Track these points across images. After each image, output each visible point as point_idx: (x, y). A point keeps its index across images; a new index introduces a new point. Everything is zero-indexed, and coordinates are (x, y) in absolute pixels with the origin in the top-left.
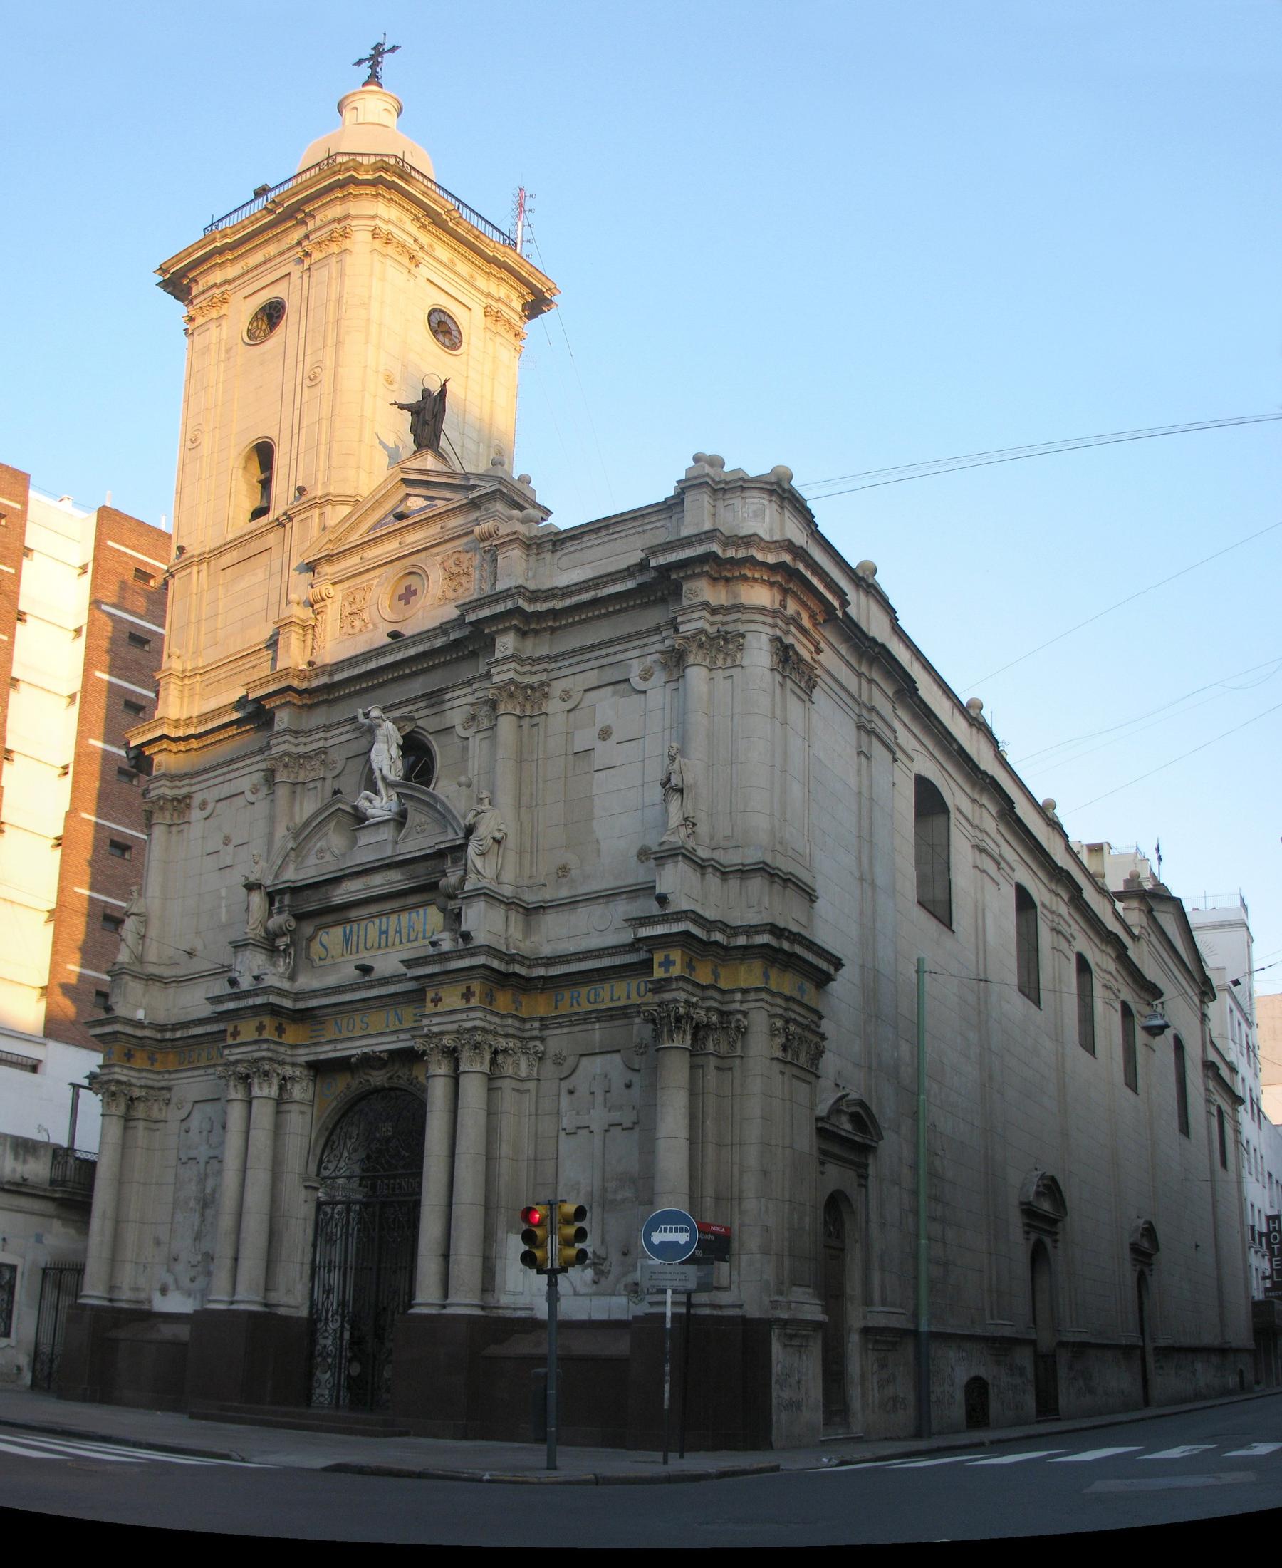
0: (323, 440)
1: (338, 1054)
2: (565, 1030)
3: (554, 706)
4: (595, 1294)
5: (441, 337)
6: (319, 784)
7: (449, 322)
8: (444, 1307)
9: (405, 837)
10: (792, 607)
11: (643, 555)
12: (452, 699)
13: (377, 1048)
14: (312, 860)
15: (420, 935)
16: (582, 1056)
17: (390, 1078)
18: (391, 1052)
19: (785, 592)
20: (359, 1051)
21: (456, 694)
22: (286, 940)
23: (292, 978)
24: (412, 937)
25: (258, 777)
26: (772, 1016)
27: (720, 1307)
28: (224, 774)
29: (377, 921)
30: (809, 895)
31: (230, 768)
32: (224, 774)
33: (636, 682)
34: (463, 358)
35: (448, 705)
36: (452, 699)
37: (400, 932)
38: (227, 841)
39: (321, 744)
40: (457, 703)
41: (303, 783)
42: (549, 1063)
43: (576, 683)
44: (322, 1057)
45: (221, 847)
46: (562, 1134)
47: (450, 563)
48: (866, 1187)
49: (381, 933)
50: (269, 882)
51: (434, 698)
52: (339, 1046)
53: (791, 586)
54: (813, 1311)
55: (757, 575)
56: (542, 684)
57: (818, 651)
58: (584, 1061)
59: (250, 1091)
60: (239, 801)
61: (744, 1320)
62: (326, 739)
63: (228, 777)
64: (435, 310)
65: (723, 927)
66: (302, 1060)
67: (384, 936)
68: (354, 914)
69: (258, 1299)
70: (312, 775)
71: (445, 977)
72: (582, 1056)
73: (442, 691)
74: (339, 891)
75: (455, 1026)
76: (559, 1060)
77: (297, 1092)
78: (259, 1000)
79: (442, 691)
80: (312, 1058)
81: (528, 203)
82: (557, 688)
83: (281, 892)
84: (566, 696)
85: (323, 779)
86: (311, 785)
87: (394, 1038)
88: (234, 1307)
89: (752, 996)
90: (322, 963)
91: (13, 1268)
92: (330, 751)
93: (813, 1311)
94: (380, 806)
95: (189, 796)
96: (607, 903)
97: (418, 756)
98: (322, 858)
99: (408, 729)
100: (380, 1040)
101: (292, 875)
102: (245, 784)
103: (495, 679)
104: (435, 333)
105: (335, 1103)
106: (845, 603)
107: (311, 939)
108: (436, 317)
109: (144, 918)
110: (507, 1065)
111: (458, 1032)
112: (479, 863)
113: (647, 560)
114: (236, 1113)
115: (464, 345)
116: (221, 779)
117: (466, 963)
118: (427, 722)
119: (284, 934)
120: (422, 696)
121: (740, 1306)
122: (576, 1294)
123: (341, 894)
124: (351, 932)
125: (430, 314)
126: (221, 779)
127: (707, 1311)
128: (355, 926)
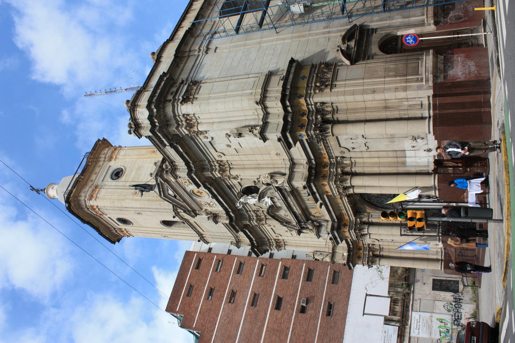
0: (162, 193)
2: (332, 151)
4: (427, 139)
5: (120, 175)
7: (115, 173)
8: (435, 188)
10: (170, 97)
13: (347, 201)
16: (340, 146)
19: (166, 101)
20: (349, 206)
23: (327, 221)
26: (315, 93)
27: (429, 104)
30: (270, 75)
33: (210, 139)
34: (126, 166)
42: (344, 155)
43: (215, 154)
46: (368, 150)
47: (186, 184)
48: (376, 29)
53: (162, 100)
54: (428, 61)
55: (162, 113)
57: (183, 81)
58: (342, 145)
59: (366, 234)
60: (274, 228)
61: (434, 96)
64: (112, 178)
65: (285, 119)
66: (354, 218)
68: (304, 207)
70: (262, 214)
72: (340, 146)
74: (297, 212)
75: (336, 189)
76: (342, 152)
77: (365, 219)
81: (89, 93)
89: (309, 102)
91: (434, 280)
93: (428, 61)
94: (267, 201)
95: (275, 240)
97: (249, 191)
99: (242, 194)
101: (294, 222)
102: (269, 228)
104: (119, 177)
106: (164, 74)
107: (314, 216)
108: (114, 177)
109: (315, 253)
110: (348, 169)
112: (280, 183)
115: (122, 167)
121: (429, 97)
122: (427, 144)
125: (113, 179)
127: (431, 111)
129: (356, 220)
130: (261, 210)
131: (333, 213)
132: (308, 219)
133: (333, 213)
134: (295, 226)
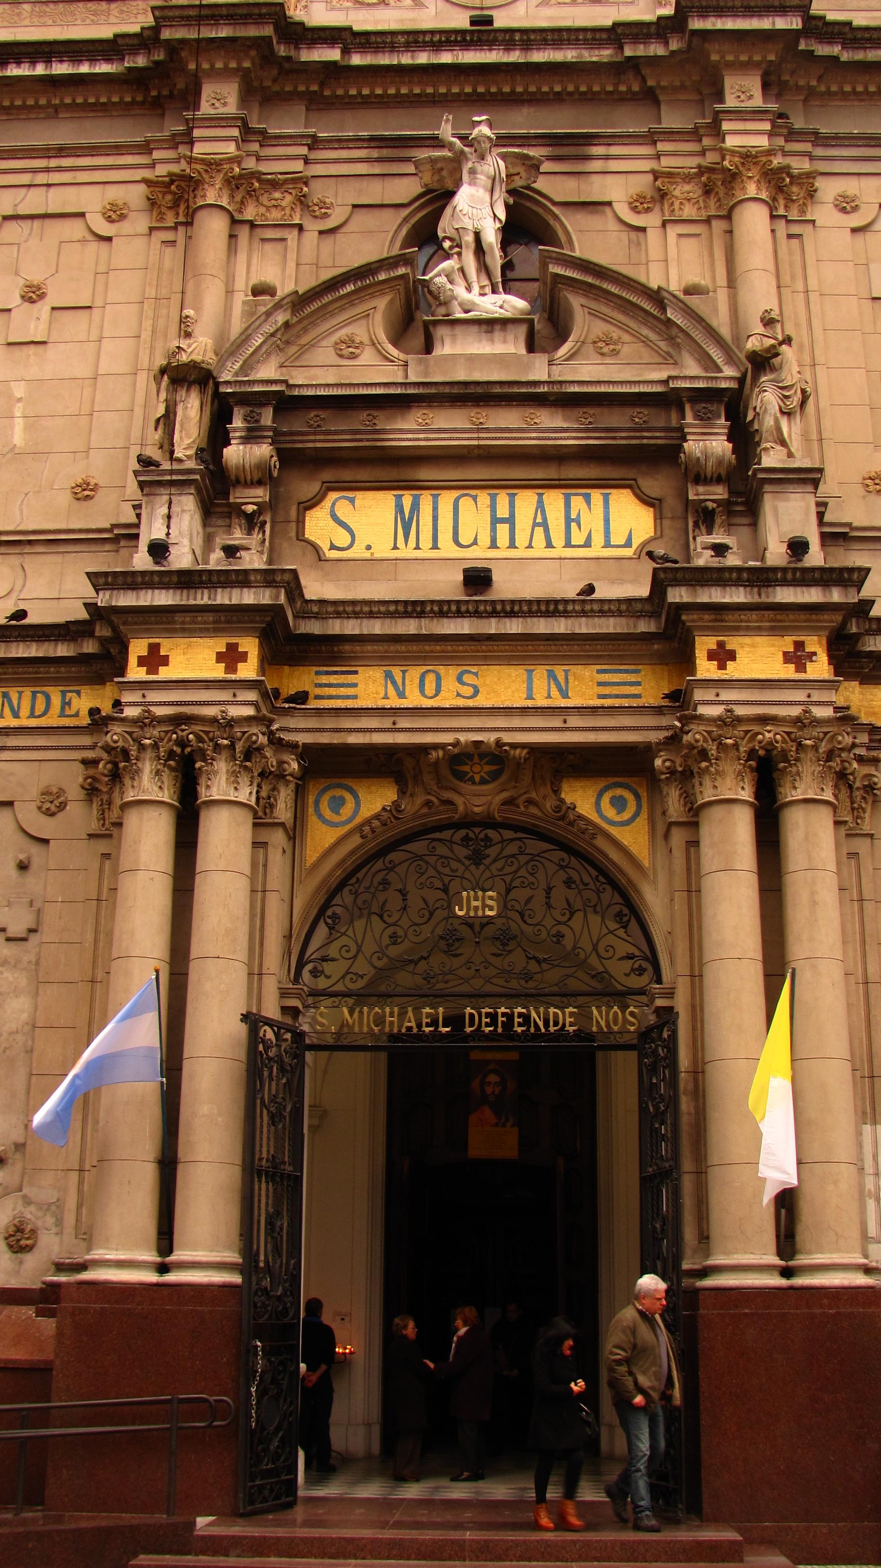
1: (401, 739)
3: (824, 213)
6: (292, 236)
9: (571, 357)
11: (150, 21)
12: (607, 158)
13: (507, 738)
14: (325, 354)
15: (598, 539)
17: (510, 802)
18: (533, 749)
21: (615, 150)
22: (261, 494)
24: (578, 538)
25: (642, 184)
28: (35, 171)
29: (484, 497)
31: (53, 163)
32: (35, 171)
35: (596, 166)
36: (607, 158)
37: (545, 525)
38: (33, 294)
39: (298, 166)
40: (613, 165)
41: (252, 225)
44: (353, 739)
45: (15, 301)
49: (495, 521)
50: (226, 376)
51: (571, 147)
52: (403, 723)
56: (811, 175)
60: (74, 229)
62: (812, 158)
63: (41, 178)
66: (302, 739)
67: (503, 530)
68: (425, 474)
69: (233, 1257)
70: (275, 216)
71: (754, 615)
73: (589, 139)
75: (795, 711)
78: (248, 597)
79: (589, 139)
80: (325, 739)
82: (829, 189)
83: (252, 401)
84: (846, 205)
85: (300, 228)
86: (270, 234)
87: (557, 722)
88: (172, 1277)
90: (334, 554)
92: (314, 184)
96: (491, 332)
98: (353, 356)
100: (516, 722)
102: (91, 200)
103: (199, 149)
105: (356, 840)
107: (313, 503)
111: (797, 721)
113: (156, 29)
114: (149, 837)
116: (25, 179)
117: (813, 595)
118: (554, 186)
119: (260, 483)
120: (372, 139)
123: (408, 430)
124: (415, 507)
126: (25, 179)
128: (426, 500)
129: (292, 747)
130: (313, 227)
131: (409, 627)
132: (292, 459)
133: (409, 627)
134: (246, 367)
